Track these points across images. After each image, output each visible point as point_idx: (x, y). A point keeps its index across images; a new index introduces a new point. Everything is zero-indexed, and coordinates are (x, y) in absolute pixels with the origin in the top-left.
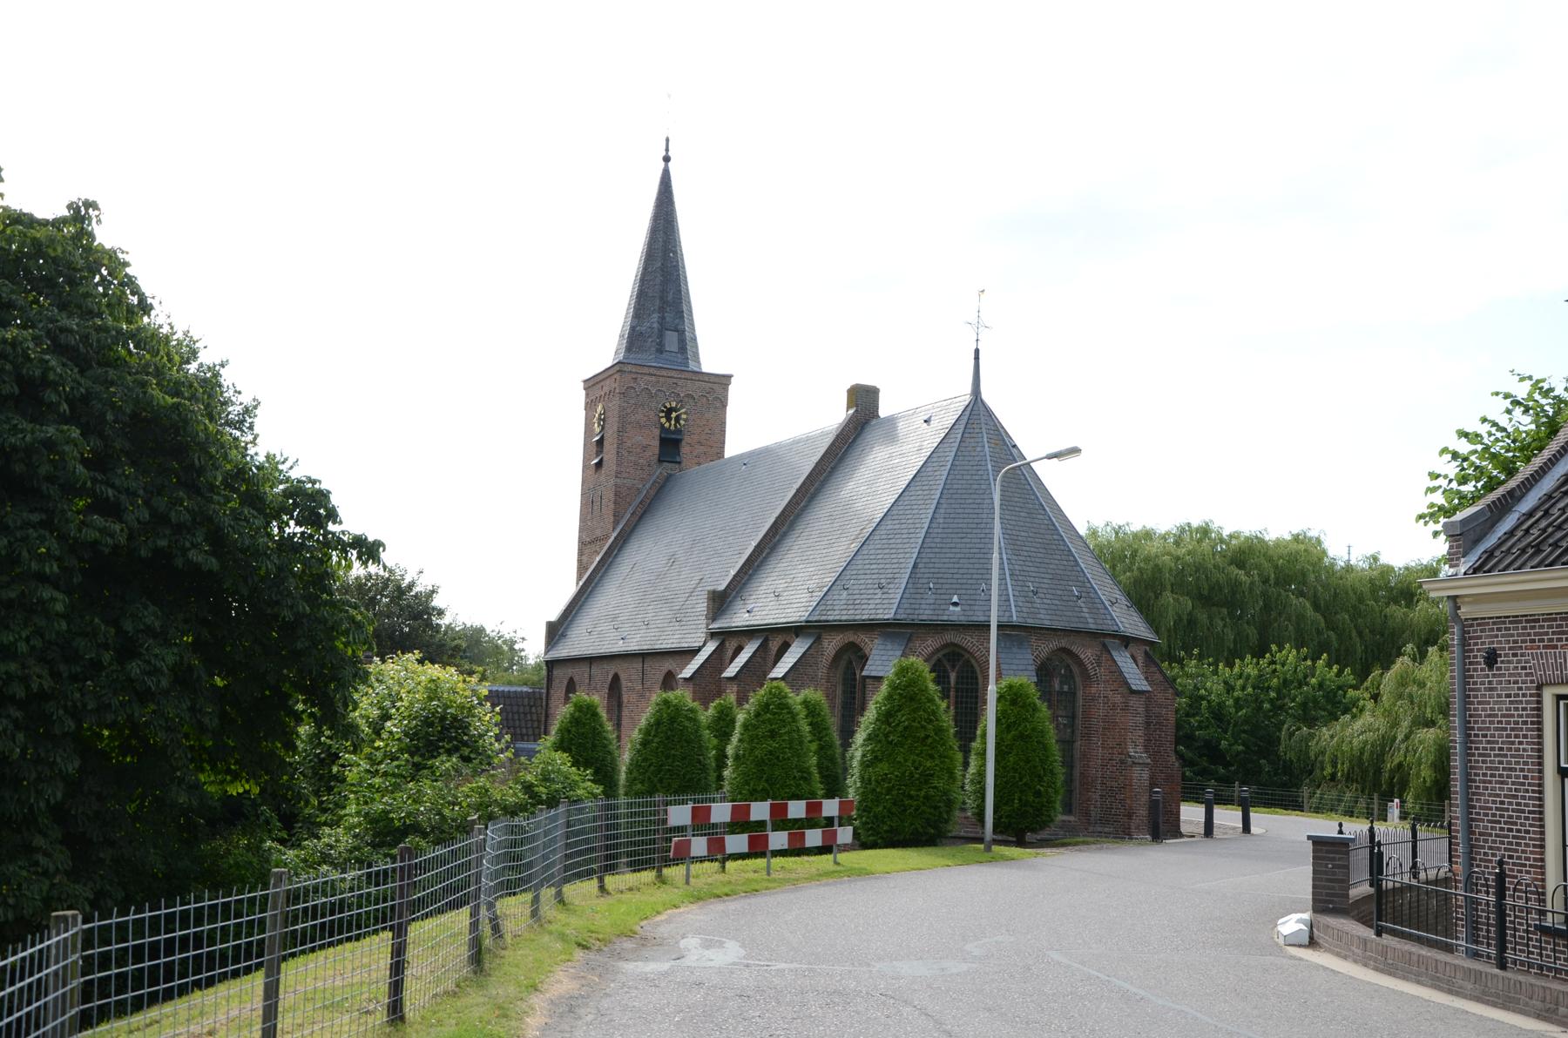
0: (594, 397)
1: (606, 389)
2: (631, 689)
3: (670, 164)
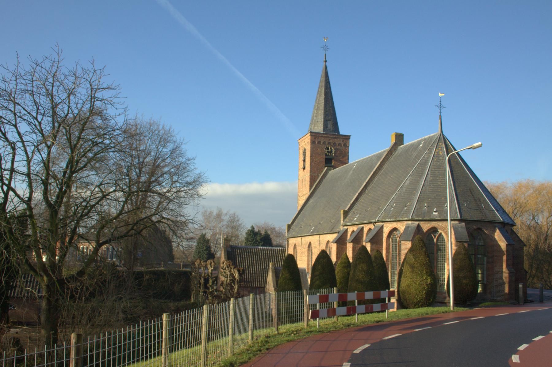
0: (302, 146)
1: (306, 142)
2: (315, 247)
3: (327, 63)
